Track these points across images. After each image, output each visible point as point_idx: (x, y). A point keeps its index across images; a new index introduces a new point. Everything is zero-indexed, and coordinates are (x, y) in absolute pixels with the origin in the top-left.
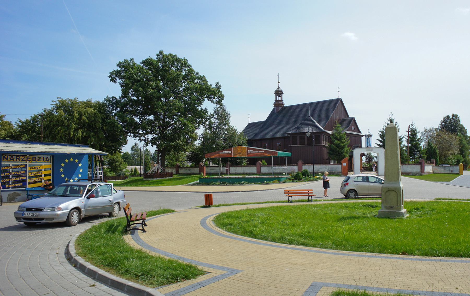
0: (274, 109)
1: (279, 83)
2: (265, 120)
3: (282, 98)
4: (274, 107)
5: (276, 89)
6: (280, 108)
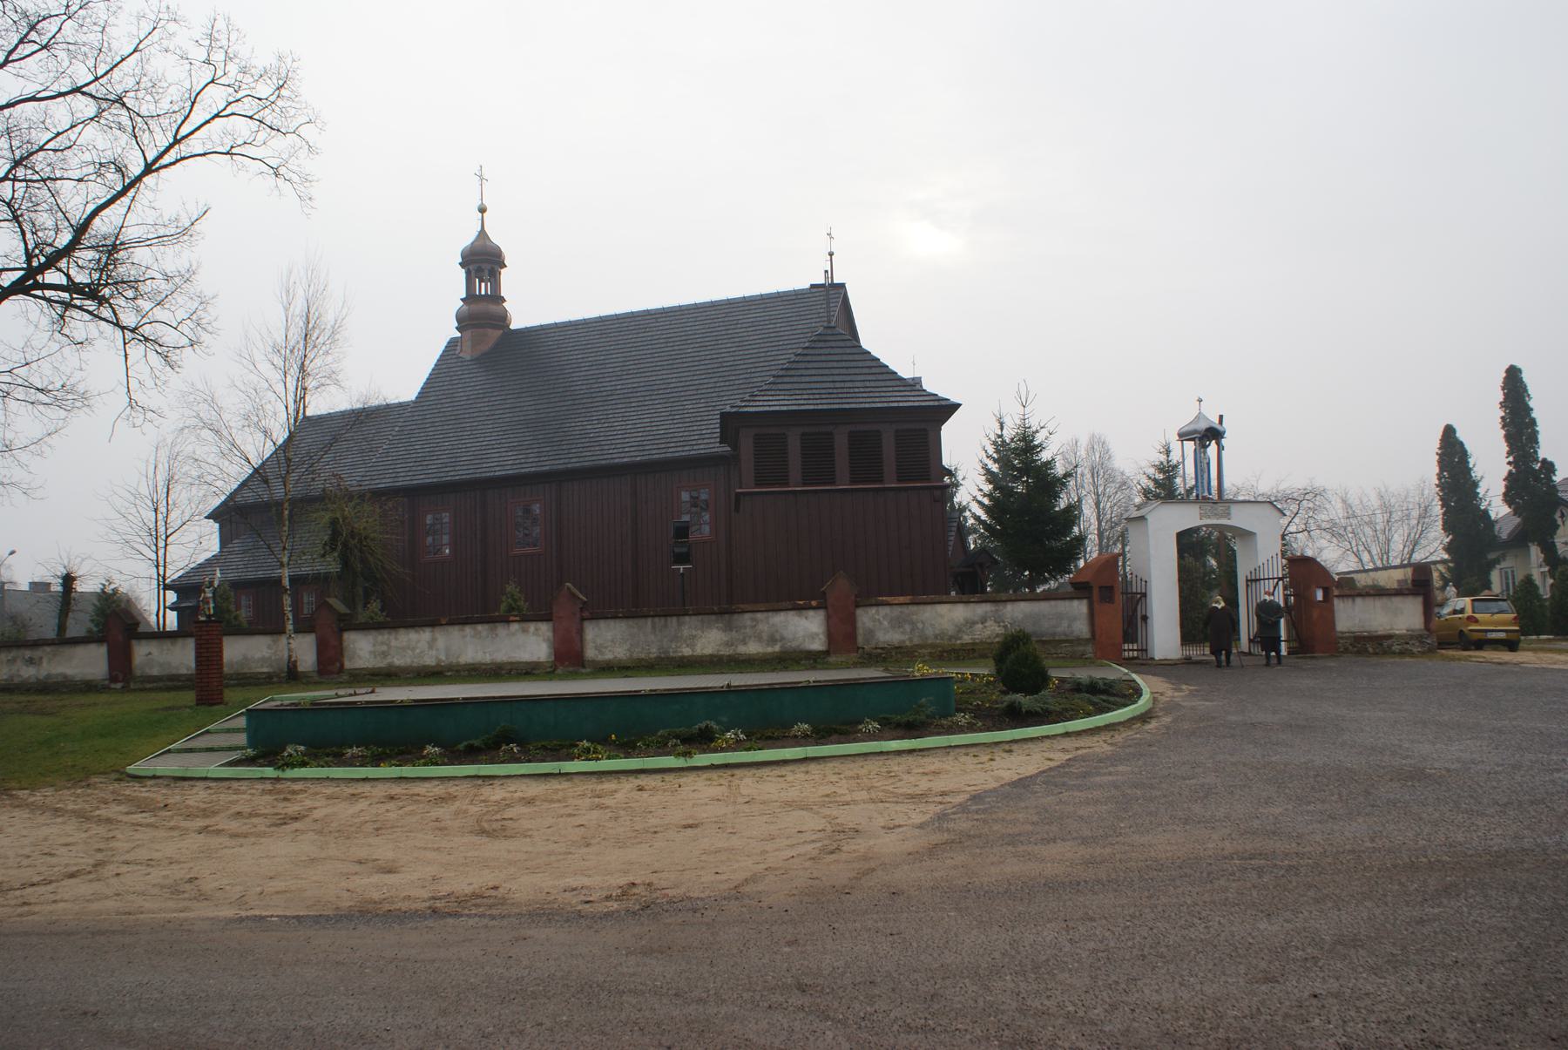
0: (452, 343)
1: (482, 210)
2: (413, 398)
3: (496, 285)
4: (458, 334)
5: (468, 238)
6: (496, 334)
